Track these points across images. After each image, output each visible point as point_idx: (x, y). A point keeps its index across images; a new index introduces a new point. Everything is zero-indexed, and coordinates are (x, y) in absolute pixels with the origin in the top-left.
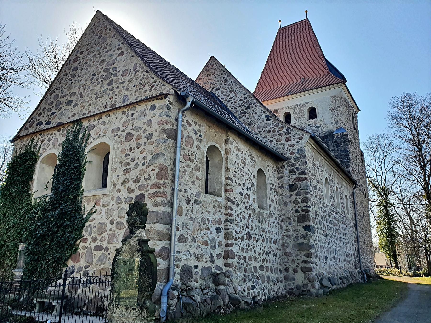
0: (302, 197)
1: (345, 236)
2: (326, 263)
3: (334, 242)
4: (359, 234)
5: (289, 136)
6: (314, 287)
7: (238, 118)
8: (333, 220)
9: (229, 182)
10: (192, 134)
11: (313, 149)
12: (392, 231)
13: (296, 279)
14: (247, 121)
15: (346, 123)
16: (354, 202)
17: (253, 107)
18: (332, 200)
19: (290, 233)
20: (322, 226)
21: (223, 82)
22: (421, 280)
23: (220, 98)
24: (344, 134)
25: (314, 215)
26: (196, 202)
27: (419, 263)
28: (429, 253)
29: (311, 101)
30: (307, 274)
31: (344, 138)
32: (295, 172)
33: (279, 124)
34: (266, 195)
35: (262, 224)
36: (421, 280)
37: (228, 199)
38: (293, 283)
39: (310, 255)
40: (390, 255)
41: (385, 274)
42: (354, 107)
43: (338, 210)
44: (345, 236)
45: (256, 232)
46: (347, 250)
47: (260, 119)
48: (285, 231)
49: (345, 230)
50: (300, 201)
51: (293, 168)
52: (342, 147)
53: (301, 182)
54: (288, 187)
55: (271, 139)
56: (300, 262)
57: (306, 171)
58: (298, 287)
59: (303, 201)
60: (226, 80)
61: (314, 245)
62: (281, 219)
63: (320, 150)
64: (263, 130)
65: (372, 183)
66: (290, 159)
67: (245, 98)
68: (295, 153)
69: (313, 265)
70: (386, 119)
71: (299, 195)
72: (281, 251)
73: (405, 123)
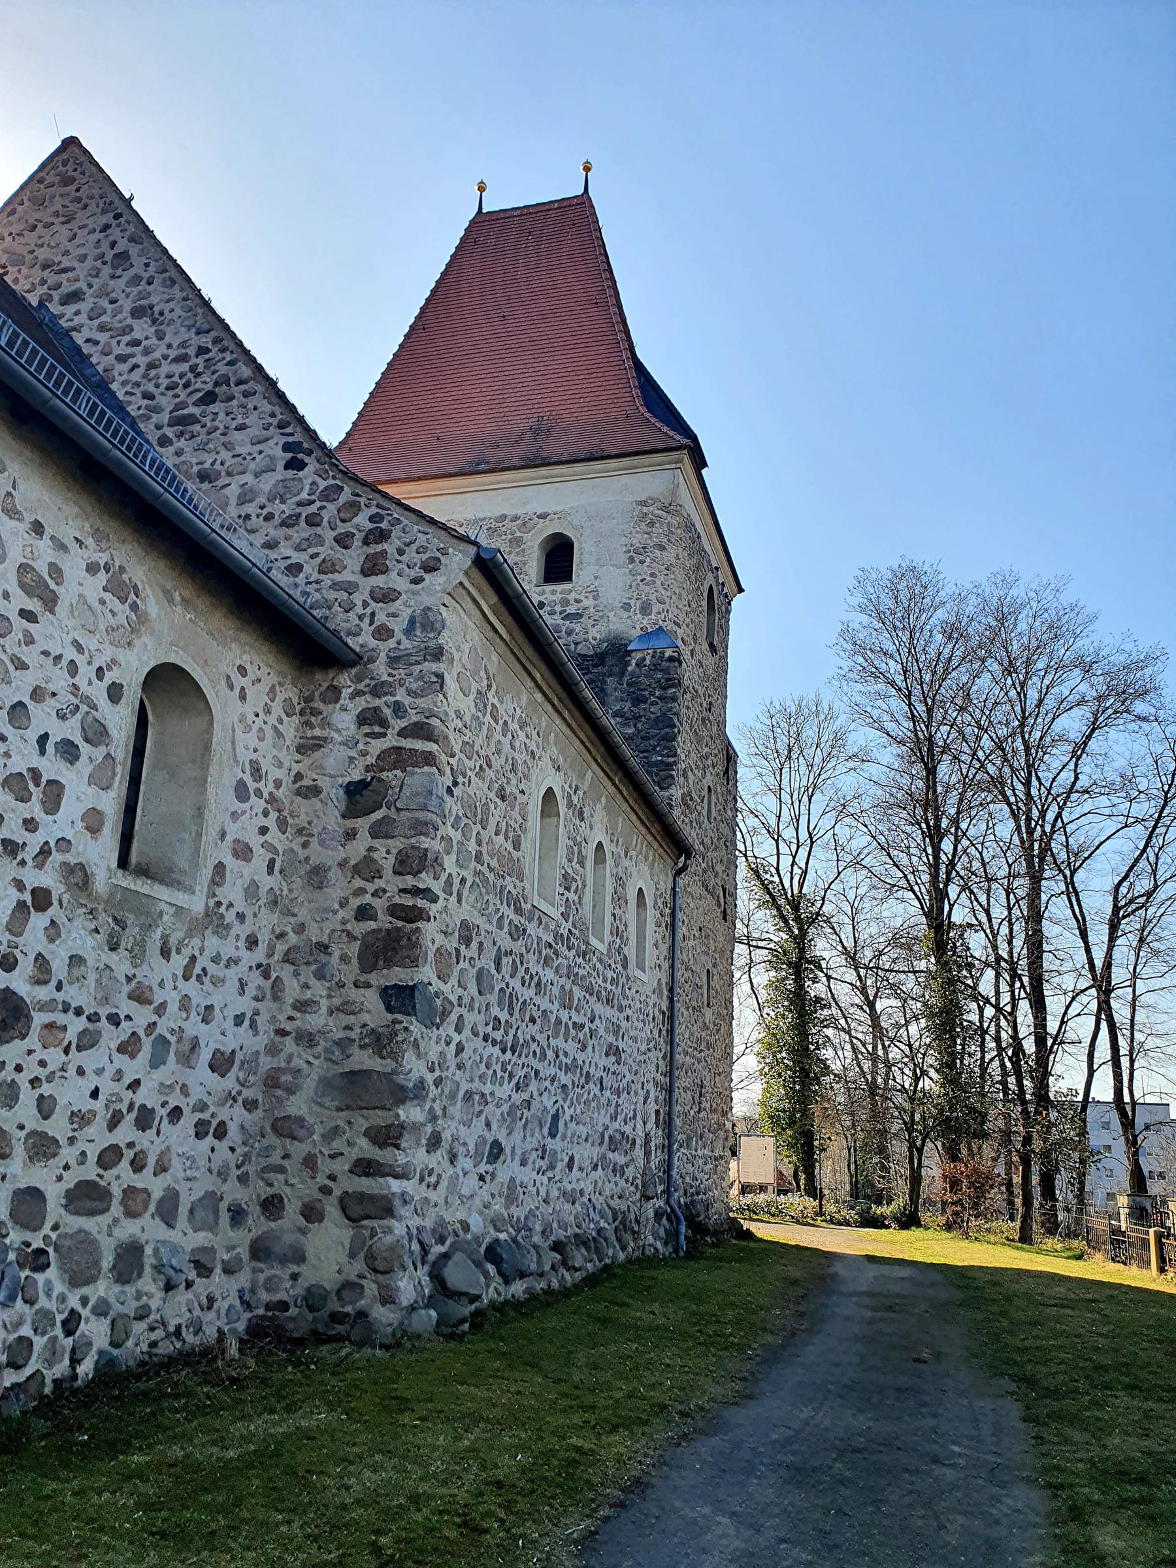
0: (396, 844)
1: (613, 1059)
2: (493, 1176)
3: (553, 1081)
4: (680, 1058)
5: (379, 548)
6: (388, 1298)
7: (155, 443)
8: (562, 981)
11: (491, 634)
12: (808, 1057)
13: (310, 1256)
14: (194, 460)
15: (682, 617)
16: (672, 927)
17: (231, 398)
18: (572, 896)
19: (316, 1020)
20: (493, 998)
21: (105, 263)
22: (884, 1242)
23: (79, 338)
24: (667, 655)
25: (452, 943)
27: (883, 1177)
28: (918, 1143)
29: (559, 508)
30: (367, 1233)
31: (665, 671)
32: (384, 723)
33: (341, 489)
34: (200, 811)
35: (137, 955)
36: (884, 1242)
38: (295, 1277)
39: (393, 1133)
40: (790, 1146)
41: (765, 1217)
42: (726, 583)
43: (594, 942)
44: (613, 1059)
45: (75, 995)
46: (614, 1118)
47: (259, 458)
48: (291, 1013)
49: (616, 1033)
50: (388, 864)
51: (377, 702)
52: (652, 704)
54: (341, 792)
55: (296, 557)
56: (342, 1166)
57: (435, 722)
58: (313, 1299)
59: (402, 862)
60: (123, 257)
61: (422, 1081)
62: (281, 948)
63: (530, 652)
64: (265, 512)
65: (759, 877)
66: (372, 660)
67: (202, 351)
68: (399, 635)
69: (405, 1183)
70: (832, 651)
71: (388, 836)
72: (259, 1113)
73: (892, 671)
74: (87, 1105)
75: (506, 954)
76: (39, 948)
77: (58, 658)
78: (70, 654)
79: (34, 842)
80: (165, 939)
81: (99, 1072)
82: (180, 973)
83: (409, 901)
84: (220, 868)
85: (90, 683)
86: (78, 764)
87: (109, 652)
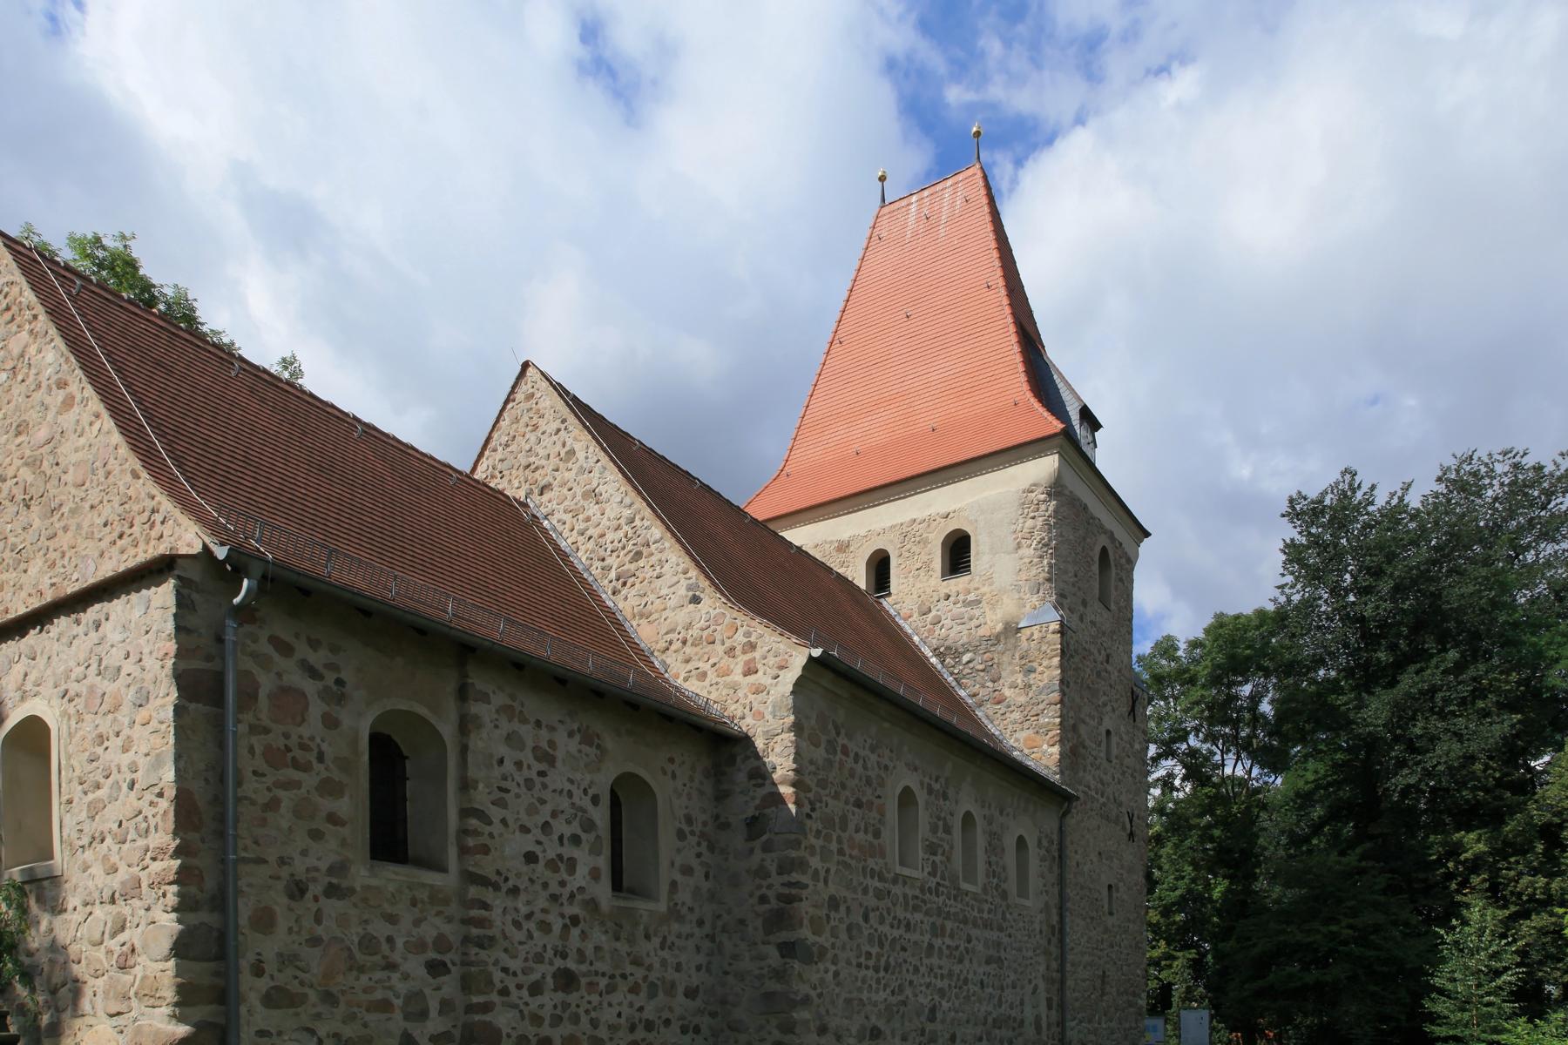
9: (474, 822)
10: (296, 679)
25: (823, 912)
26: (332, 891)
35: (631, 941)
37: (472, 878)
50: (773, 869)
53: (777, 807)
62: (720, 923)
74: (615, 1020)
75: (873, 910)
76: (578, 945)
77: (562, 791)
78: (568, 786)
79: (566, 892)
80: (646, 929)
81: (620, 1004)
82: (658, 946)
83: (786, 891)
84: (674, 884)
85: (581, 799)
86: (582, 845)
87: (588, 777)
